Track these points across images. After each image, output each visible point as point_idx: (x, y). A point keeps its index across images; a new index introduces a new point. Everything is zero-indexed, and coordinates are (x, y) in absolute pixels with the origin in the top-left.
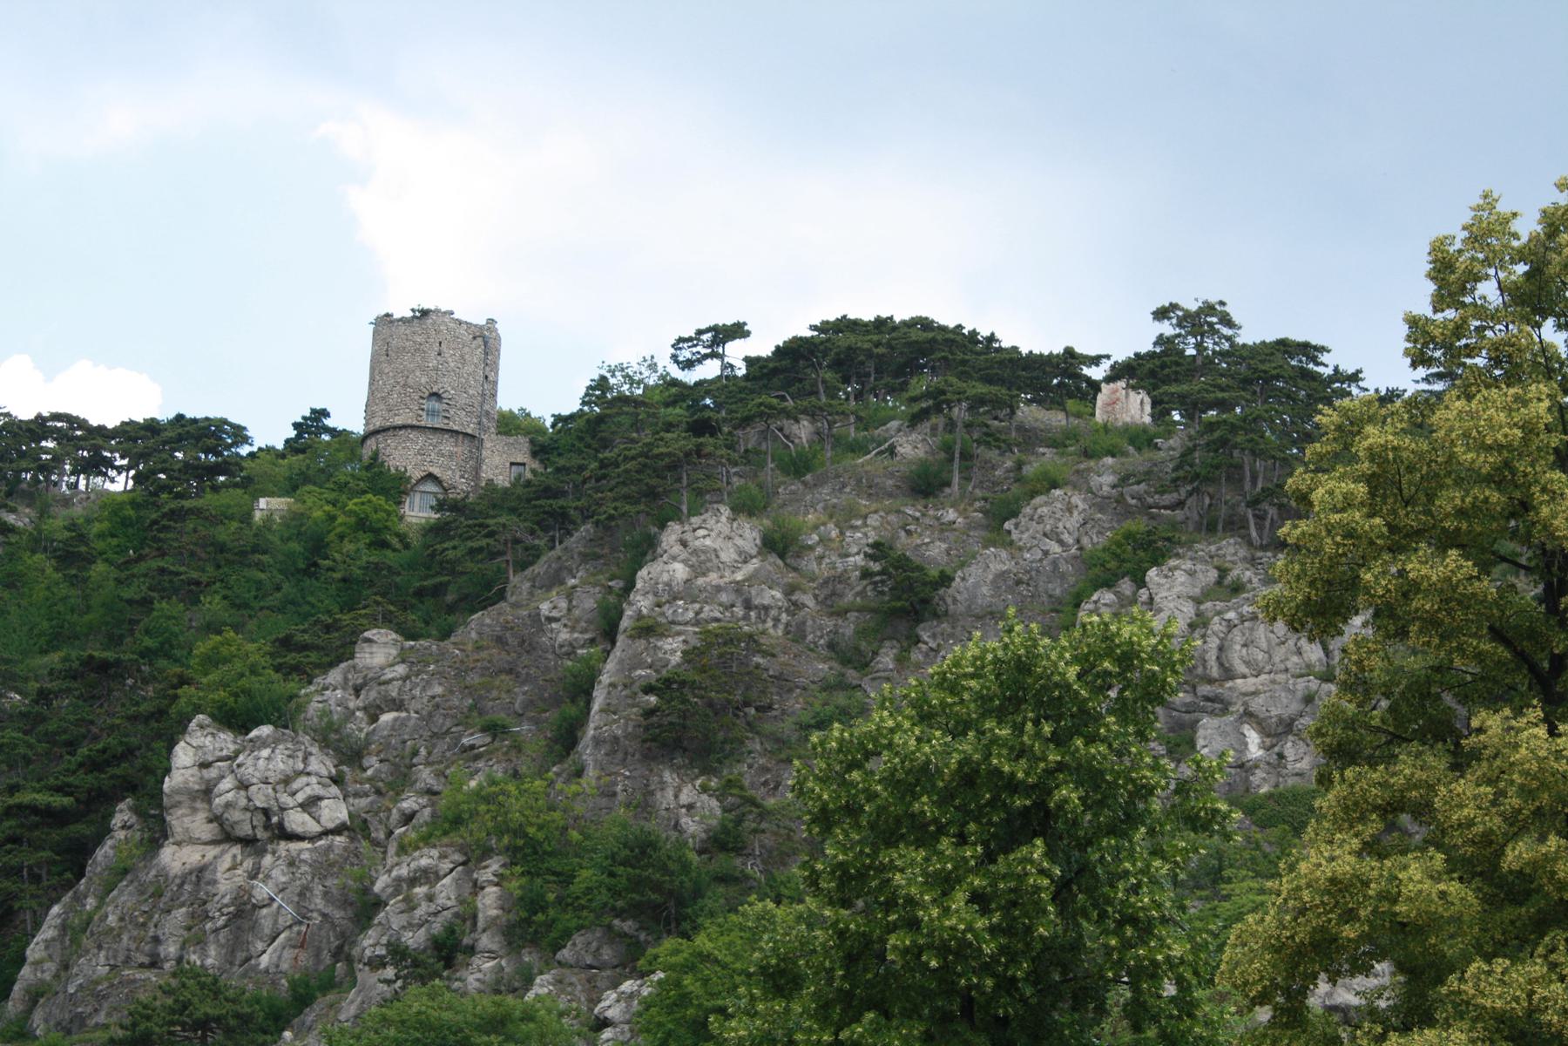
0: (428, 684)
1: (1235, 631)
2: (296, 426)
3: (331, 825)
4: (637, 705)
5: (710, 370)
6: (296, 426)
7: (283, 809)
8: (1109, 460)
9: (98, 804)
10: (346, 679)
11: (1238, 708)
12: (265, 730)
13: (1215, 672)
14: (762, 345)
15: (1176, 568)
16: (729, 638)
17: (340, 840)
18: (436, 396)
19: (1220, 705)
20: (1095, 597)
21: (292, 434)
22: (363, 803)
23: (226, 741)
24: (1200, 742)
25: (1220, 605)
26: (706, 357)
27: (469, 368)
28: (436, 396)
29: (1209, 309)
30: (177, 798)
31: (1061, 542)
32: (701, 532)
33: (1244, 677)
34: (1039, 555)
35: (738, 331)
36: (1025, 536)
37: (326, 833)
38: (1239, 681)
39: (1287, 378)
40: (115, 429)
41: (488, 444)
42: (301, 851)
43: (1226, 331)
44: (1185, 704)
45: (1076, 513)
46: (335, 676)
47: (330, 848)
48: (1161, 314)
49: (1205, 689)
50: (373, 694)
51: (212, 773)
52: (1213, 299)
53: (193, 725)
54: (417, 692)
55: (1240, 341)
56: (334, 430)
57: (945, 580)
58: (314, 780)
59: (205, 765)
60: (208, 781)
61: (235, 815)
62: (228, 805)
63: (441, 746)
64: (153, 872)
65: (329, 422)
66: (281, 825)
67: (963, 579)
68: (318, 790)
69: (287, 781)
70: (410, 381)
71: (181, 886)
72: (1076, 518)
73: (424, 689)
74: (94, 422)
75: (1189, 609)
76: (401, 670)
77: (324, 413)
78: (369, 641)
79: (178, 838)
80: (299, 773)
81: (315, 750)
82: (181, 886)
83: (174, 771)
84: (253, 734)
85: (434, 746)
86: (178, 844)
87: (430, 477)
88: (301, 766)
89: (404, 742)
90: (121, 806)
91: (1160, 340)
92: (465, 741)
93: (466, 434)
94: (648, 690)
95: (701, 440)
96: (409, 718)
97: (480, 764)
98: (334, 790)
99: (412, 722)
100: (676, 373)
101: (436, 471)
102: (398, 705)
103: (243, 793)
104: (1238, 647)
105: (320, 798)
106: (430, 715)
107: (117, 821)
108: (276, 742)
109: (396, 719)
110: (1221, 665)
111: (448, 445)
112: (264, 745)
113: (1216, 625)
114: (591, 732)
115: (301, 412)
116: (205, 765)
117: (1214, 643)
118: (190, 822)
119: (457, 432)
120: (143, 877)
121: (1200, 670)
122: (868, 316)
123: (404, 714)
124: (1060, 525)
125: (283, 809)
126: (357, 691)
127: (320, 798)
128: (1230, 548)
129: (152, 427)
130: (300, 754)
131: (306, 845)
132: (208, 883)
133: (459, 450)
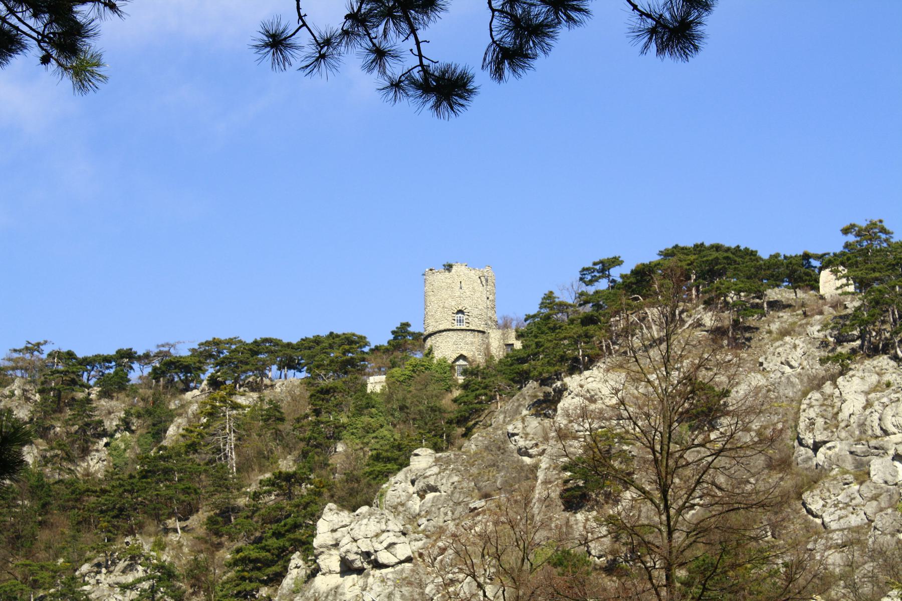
0: (450, 476)
1: (887, 408)
2: (393, 332)
3: (403, 558)
4: (560, 478)
5: (603, 285)
6: (393, 332)
7: (376, 551)
8: (818, 317)
9: (283, 556)
10: (406, 477)
11: (892, 452)
12: (364, 509)
13: (878, 432)
14: (626, 269)
15: (853, 376)
16: (608, 436)
17: (408, 565)
18: (460, 312)
19: (881, 450)
20: (809, 396)
21: (391, 337)
22: (420, 544)
23: (345, 517)
24: (872, 473)
25: (879, 394)
26: (600, 277)
27: (479, 294)
28: (460, 312)
29: (873, 225)
30: (321, 550)
31: (791, 367)
32: (590, 380)
33: (895, 434)
34: (779, 374)
35: (615, 262)
36: (771, 365)
37: (401, 562)
38: (892, 436)
39: (210, 519)
40: (297, 344)
41: (492, 335)
42: (387, 574)
43: (883, 236)
44: (863, 452)
45: (798, 349)
46: (400, 476)
47: (402, 571)
48: (846, 231)
49: (873, 442)
50: (421, 484)
51: (337, 535)
52: (875, 219)
53: (326, 510)
54: (444, 481)
55: (893, 240)
56: (414, 333)
57: (726, 393)
58: (391, 534)
59: (334, 531)
60: (336, 540)
61: (351, 557)
62: (348, 551)
63: (460, 509)
64: (312, 591)
65: (410, 329)
66: (376, 561)
67: (737, 392)
68: (394, 540)
69: (377, 536)
70: (446, 305)
71: (327, 597)
72: (799, 352)
73: (448, 479)
74: (285, 341)
75: (862, 399)
76: (436, 470)
77: (408, 325)
78: (416, 455)
79: (324, 571)
80: (383, 532)
81: (391, 517)
82: (327, 597)
83: (318, 536)
84: (358, 512)
85: (455, 510)
86: (324, 574)
87: (462, 357)
88: (384, 527)
89: (439, 509)
90: (294, 556)
91: (847, 245)
92: (472, 506)
93: (479, 331)
94: (565, 469)
95: (588, 327)
96: (441, 496)
97: (479, 518)
98: (403, 538)
99: (442, 498)
100: (584, 288)
101: (465, 353)
102: (434, 489)
103: (354, 544)
104: (890, 417)
105: (395, 544)
106: (452, 493)
107: (292, 564)
108: (371, 514)
109: (434, 497)
110: (882, 429)
111: (469, 337)
112: (364, 517)
113: (877, 406)
114: (537, 496)
115: (395, 325)
116: (334, 531)
117: (876, 416)
118: (330, 561)
119: (474, 330)
120: (307, 594)
121: (870, 432)
122: (690, 244)
123: (438, 494)
124: (790, 357)
125: (376, 551)
126: (413, 482)
127: (395, 544)
128: (883, 361)
129: (317, 341)
130: (384, 521)
131: (390, 569)
132: (341, 595)
133: (476, 340)
